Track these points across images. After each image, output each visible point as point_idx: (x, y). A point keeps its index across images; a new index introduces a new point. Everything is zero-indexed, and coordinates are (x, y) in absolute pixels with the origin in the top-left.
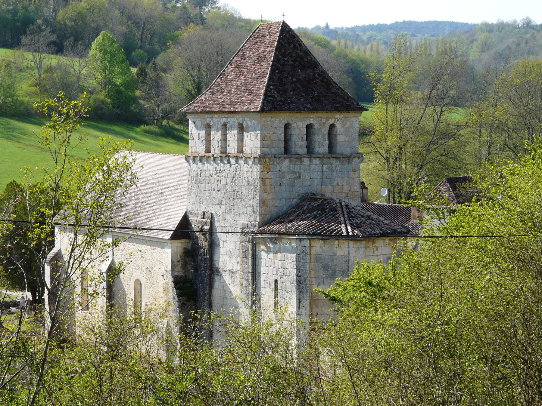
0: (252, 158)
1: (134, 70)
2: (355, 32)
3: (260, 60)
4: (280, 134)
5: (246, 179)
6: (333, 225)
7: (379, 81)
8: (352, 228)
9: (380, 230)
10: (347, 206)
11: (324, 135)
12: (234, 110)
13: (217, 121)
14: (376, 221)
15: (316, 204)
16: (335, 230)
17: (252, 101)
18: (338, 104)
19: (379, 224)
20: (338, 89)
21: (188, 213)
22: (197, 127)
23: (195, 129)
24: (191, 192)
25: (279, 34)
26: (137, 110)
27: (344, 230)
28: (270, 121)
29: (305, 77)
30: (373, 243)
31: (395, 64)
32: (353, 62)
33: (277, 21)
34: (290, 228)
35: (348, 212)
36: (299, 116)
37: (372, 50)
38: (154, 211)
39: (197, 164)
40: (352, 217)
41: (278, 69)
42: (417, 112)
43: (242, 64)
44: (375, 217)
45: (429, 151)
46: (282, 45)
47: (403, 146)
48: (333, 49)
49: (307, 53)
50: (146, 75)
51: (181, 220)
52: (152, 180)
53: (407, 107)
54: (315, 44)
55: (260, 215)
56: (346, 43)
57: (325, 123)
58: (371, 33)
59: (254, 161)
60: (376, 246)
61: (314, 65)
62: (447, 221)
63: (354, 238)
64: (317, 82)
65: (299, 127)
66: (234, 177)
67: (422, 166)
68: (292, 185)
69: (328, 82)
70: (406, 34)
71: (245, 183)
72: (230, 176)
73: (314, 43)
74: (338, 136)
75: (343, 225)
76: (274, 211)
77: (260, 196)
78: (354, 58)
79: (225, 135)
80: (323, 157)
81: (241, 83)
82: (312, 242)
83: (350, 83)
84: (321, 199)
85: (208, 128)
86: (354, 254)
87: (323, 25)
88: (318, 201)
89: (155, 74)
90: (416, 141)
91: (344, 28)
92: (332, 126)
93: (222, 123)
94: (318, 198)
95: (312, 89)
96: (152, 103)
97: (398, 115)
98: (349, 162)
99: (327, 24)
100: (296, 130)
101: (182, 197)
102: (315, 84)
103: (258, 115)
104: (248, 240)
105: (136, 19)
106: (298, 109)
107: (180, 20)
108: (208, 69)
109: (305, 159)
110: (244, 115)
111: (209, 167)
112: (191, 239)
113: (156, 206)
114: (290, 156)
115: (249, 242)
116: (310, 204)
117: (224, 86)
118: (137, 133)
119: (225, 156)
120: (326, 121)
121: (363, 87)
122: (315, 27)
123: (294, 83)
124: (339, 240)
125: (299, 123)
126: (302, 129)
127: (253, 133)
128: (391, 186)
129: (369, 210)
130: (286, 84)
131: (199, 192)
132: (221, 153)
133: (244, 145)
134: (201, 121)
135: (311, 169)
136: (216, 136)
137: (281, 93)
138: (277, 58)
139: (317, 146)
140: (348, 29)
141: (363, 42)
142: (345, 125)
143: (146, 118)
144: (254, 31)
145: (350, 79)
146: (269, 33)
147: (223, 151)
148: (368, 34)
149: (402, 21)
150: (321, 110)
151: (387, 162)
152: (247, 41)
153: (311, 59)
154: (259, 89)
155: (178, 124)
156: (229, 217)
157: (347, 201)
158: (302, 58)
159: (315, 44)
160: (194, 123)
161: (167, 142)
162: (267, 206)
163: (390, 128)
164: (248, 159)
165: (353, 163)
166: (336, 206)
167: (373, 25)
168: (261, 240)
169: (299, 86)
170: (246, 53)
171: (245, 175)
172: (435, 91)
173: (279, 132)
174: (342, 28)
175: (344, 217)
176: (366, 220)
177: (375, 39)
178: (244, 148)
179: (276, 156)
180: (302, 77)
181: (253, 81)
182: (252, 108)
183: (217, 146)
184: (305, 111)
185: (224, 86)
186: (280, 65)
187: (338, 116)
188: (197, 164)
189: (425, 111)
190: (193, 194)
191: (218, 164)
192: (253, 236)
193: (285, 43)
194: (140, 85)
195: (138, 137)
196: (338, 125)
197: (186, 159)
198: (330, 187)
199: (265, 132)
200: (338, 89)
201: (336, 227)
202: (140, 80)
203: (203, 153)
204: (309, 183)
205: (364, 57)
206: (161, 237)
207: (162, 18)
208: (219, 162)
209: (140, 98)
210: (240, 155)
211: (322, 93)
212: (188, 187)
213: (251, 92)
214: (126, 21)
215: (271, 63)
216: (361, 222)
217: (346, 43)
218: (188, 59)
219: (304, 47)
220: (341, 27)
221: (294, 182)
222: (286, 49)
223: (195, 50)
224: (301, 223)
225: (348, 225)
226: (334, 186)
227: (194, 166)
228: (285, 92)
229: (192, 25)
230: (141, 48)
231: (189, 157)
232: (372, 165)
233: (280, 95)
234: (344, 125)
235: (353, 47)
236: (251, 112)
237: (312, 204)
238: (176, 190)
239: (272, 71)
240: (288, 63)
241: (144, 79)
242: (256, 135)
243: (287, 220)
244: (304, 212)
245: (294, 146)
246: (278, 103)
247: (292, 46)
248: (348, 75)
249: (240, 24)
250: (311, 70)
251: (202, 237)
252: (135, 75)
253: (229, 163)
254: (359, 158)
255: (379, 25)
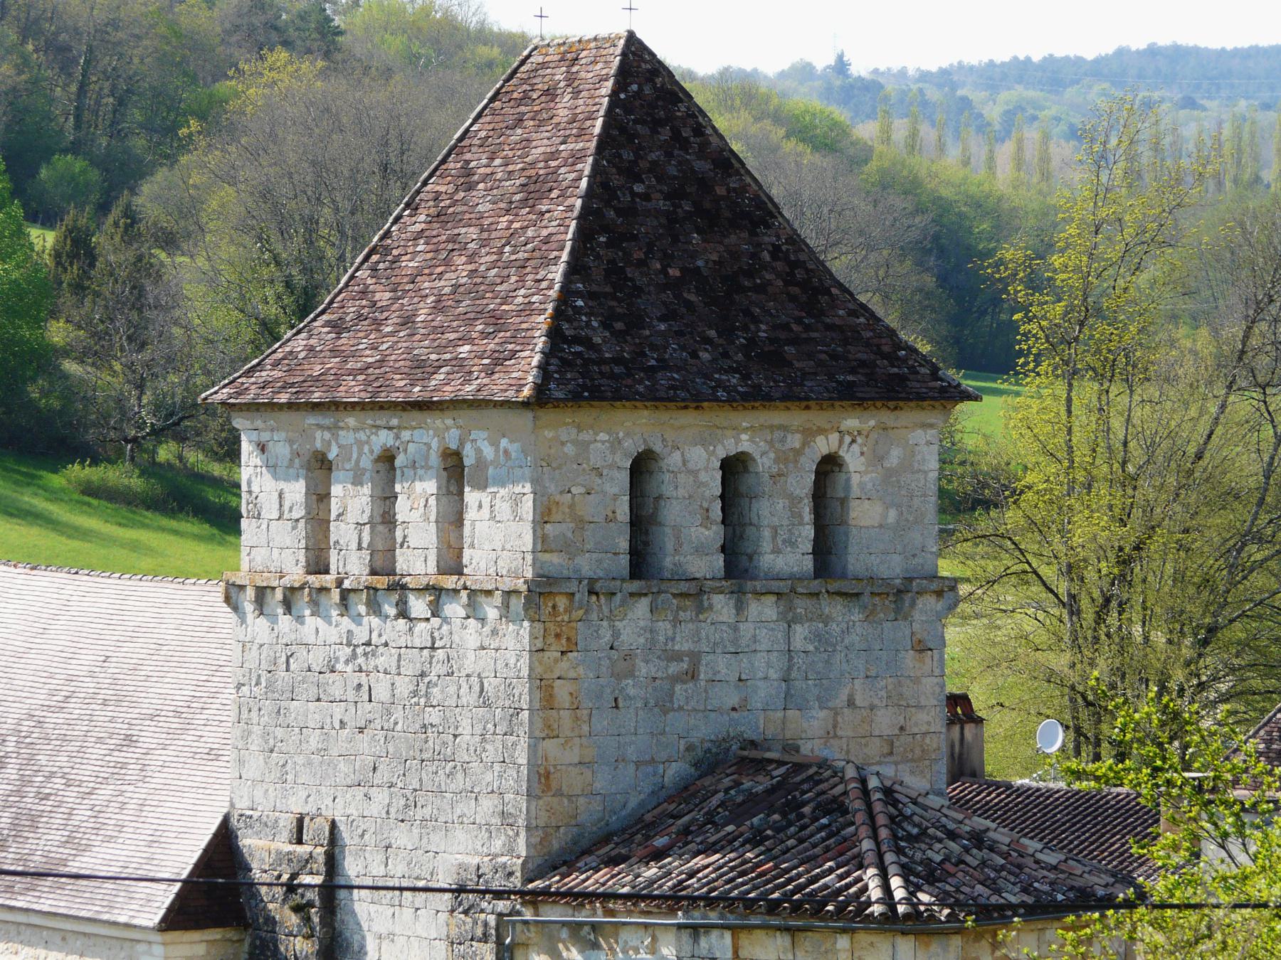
0: (498, 598)
1: (44, 239)
2: (954, 87)
3: (535, 190)
4: (615, 497)
5: (475, 680)
6: (831, 870)
7: (1035, 284)
8: (907, 883)
9: (1025, 890)
10: (888, 792)
11: (794, 501)
12: (426, 396)
13: (357, 440)
14: (1005, 856)
15: (760, 784)
16: (839, 892)
17: (498, 361)
18: (853, 371)
19: (1020, 867)
20: (853, 313)
21: (234, 821)
22: (272, 467)
23: (267, 476)
24: (246, 735)
25: (610, 84)
26: (56, 404)
27: (875, 893)
28: (575, 443)
29: (719, 263)
31: (1103, 213)
32: (943, 207)
33: (603, 33)
34: (651, 882)
35: (892, 818)
36: (689, 421)
37: (1019, 162)
38: (96, 813)
39: (273, 618)
40: (910, 838)
41: (605, 229)
42: (1193, 412)
43: (459, 209)
44: (1002, 836)
45: (1238, 570)
46: (623, 130)
47: (1137, 548)
48: (861, 156)
49: (727, 162)
50: (91, 257)
51: (206, 851)
52: (90, 685)
53: (1153, 391)
54: (788, 136)
55: (528, 828)
56: (914, 134)
57: (798, 453)
58: (1019, 92)
59: (506, 605)
61: (757, 212)
62: (1253, 849)
63: (916, 924)
64: (770, 283)
65: (691, 465)
66: (423, 675)
67: (1212, 630)
68: (664, 705)
69: (809, 283)
70: (1162, 101)
71: (469, 698)
72: (409, 669)
73: (782, 132)
74: (853, 504)
75: (871, 871)
76: (589, 812)
77: (533, 749)
78: (946, 192)
79: (386, 499)
80: (793, 590)
81: (456, 287)
82: (744, 939)
83: (928, 295)
84: (781, 763)
85: (319, 469)
87: (822, 60)
88: (768, 773)
89: (130, 255)
90: (1186, 531)
91: (911, 72)
92: (829, 466)
93: (377, 450)
94: (770, 761)
95: (747, 312)
96: (114, 374)
97: (1117, 424)
98: (897, 611)
99: (840, 58)
100: (682, 478)
101: (213, 755)
102: (761, 289)
103: (524, 419)
104: (479, 932)
105: (56, 34)
106: (687, 393)
107: (234, 39)
108: (342, 233)
109: (719, 601)
110: (465, 416)
111: (323, 631)
112: (246, 926)
113: (106, 792)
114: (654, 585)
115: (485, 939)
116: (737, 784)
117: (383, 297)
118: (55, 495)
119: (387, 587)
120: (805, 444)
121: (984, 313)
122: (793, 67)
123: (675, 286)
124: (854, 931)
125: (693, 449)
126: (703, 477)
127: (503, 492)
128: (1084, 714)
129: (985, 811)
130: (639, 290)
131: (279, 732)
132: (373, 572)
133: (467, 541)
134: (291, 442)
135: (743, 642)
136: (351, 502)
137: (619, 326)
138: (605, 185)
139: (766, 546)
140: (924, 76)
141: (983, 127)
142: (881, 459)
143: (91, 435)
144: (520, 77)
145: (930, 281)
146: (571, 79)
147: (378, 565)
148: (1004, 96)
149: (1143, 46)
150: (785, 398)
151: (1071, 613)
152: (480, 115)
153: (745, 188)
154: (528, 310)
155: (220, 460)
156: (402, 837)
157: (888, 771)
158: (704, 184)
159: (788, 136)
160: (262, 448)
161: (176, 532)
162: (559, 793)
163: (1080, 476)
164: (482, 599)
165: (917, 615)
166: (845, 793)
167: (1028, 59)
168: (533, 934)
169: (692, 298)
170: (477, 160)
171: (470, 663)
172: (1263, 326)
173: (612, 489)
174: (903, 73)
175: (875, 837)
176: (967, 850)
177: (1034, 118)
178: (467, 553)
179: (598, 586)
180: (703, 264)
181: (505, 279)
182: (499, 387)
183: (354, 546)
184: (717, 400)
185: (383, 297)
187: (851, 422)
188: (273, 618)
189: (1223, 407)
190: (256, 743)
191: (357, 619)
192: (500, 915)
193: (636, 122)
194: (67, 299)
195: (55, 510)
196: (854, 460)
197: (227, 599)
198: (822, 714)
199: (552, 488)
200: (853, 313)
201: (841, 878)
202: (66, 278)
203: (296, 574)
204: (734, 700)
205: (986, 187)
206: (122, 919)
207: (162, 30)
208: (362, 609)
209: (66, 352)
210: (450, 582)
211: (786, 327)
212: (234, 714)
213: (496, 321)
214: (14, 37)
215: (579, 203)
216: (946, 859)
217: (914, 134)
218: (266, 194)
219: (714, 139)
220: (896, 66)
222: (640, 147)
223: (292, 158)
224: (699, 861)
225: (892, 869)
227: (259, 627)
228: (635, 321)
229: (282, 55)
230: (75, 148)
231: (242, 588)
232: (1008, 626)
233: (615, 333)
234: (877, 458)
235: (941, 148)
236: (496, 404)
237: (747, 784)
238: (187, 726)
239: (584, 236)
240: (649, 205)
241: (85, 275)
242: (516, 501)
243: (641, 852)
244: (710, 819)
245: (670, 545)
246: (605, 368)
247: (665, 134)
248: (919, 263)
249: (484, 52)
250: (745, 235)
251: (293, 920)
252: (47, 259)
253: (403, 614)
254: (939, 594)
255: (1050, 60)
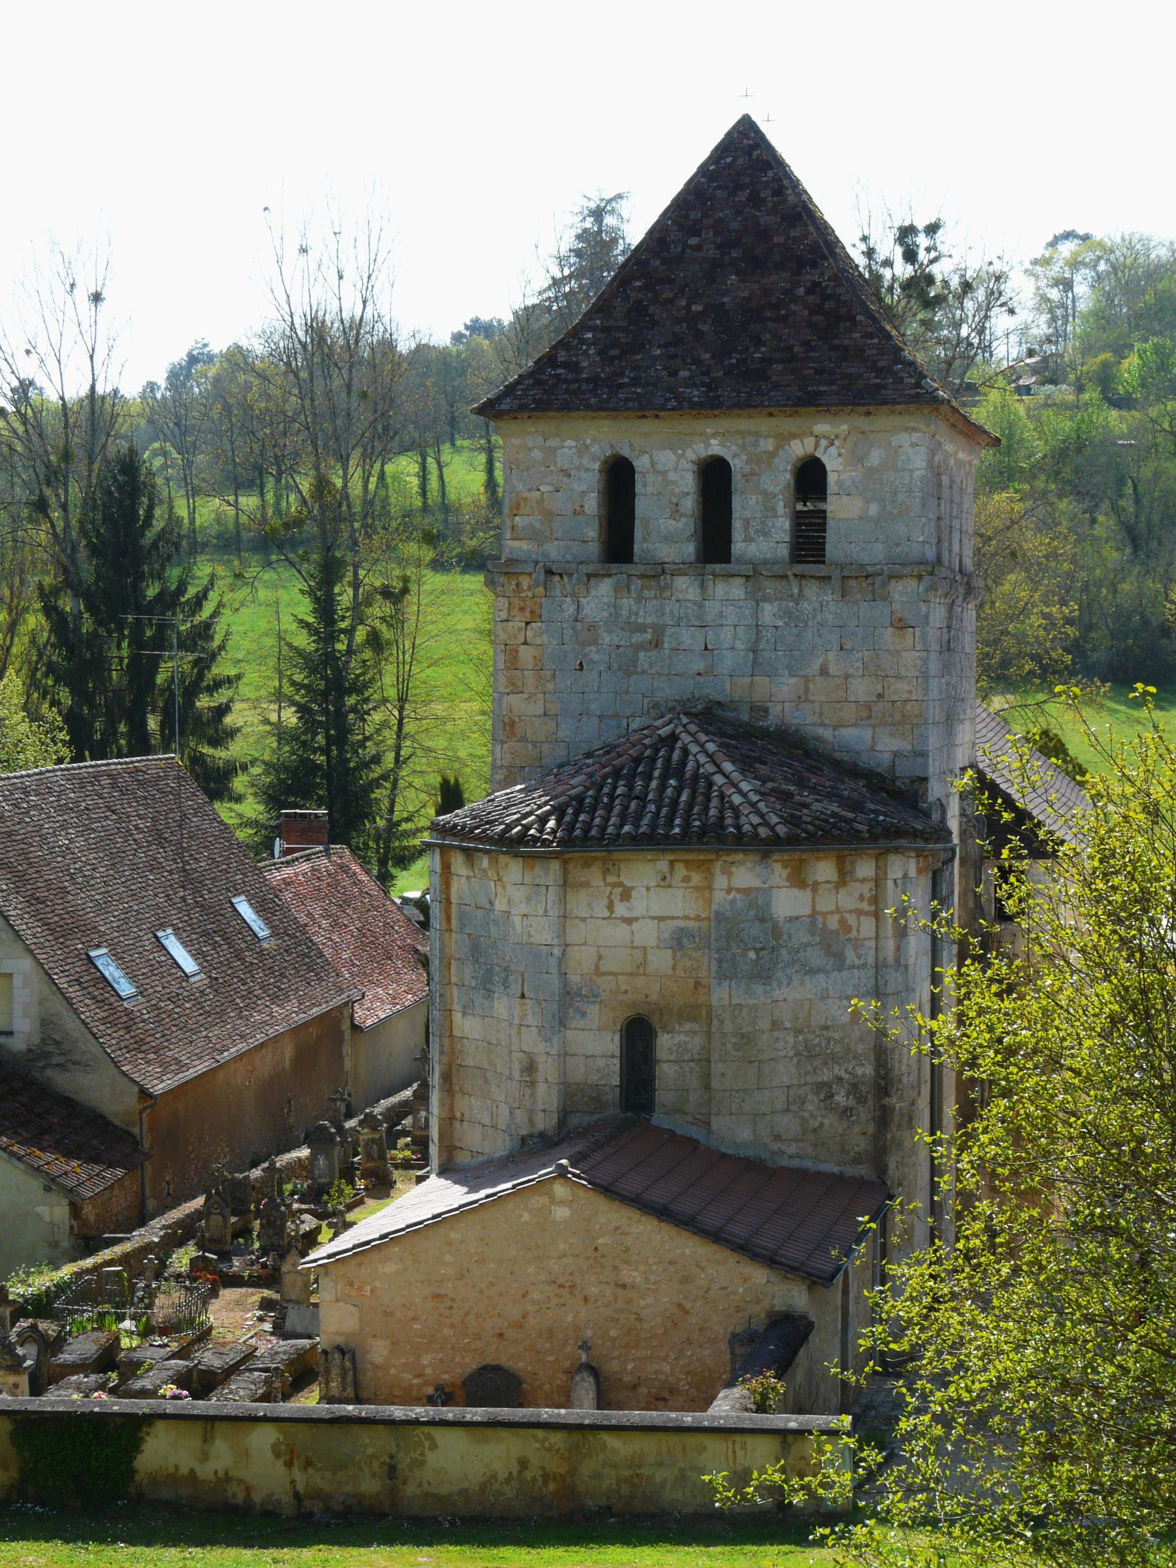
11: (768, 496)
29: (748, 299)
30: (606, 872)
57: (772, 455)
60: (621, 884)
65: (659, 467)
68: (628, 668)
86: (524, 908)
100: (650, 478)
106: (646, 404)
120: (778, 447)
135: (709, 618)
142: (860, 460)
162: (523, 739)
186: (664, 262)
196: (832, 462)
198: (792, 681)
204: (699, 665)
219: (792, 199)
221: (635, 661)
226: (807, 679)
